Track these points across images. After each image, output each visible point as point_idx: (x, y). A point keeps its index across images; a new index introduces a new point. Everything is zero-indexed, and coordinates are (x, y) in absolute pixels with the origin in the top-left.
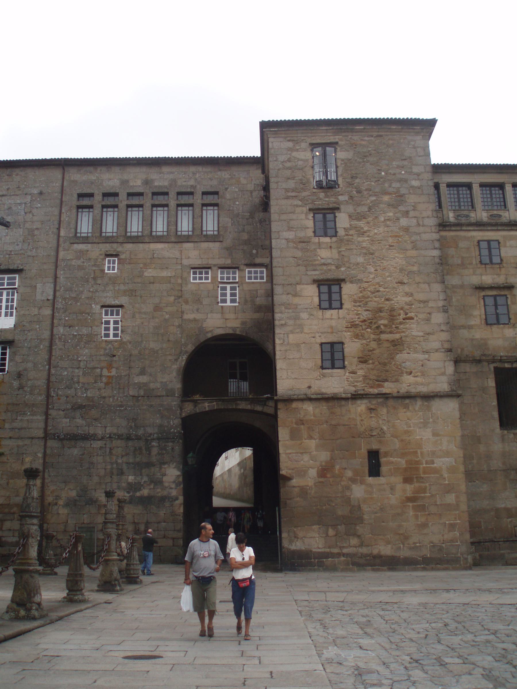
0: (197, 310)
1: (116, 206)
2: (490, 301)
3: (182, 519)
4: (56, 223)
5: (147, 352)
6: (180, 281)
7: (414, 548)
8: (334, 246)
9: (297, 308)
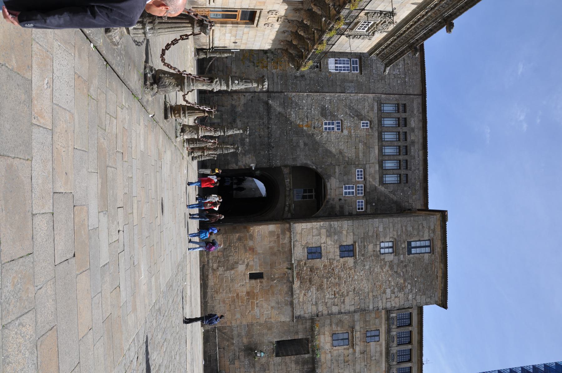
0: (341, 173)
1: (399, 126)
2: (346, 336)
4: (389, 92)
5: (317, 147)
6: (357, 163)
7: (212, 297)
8: (375, 253)
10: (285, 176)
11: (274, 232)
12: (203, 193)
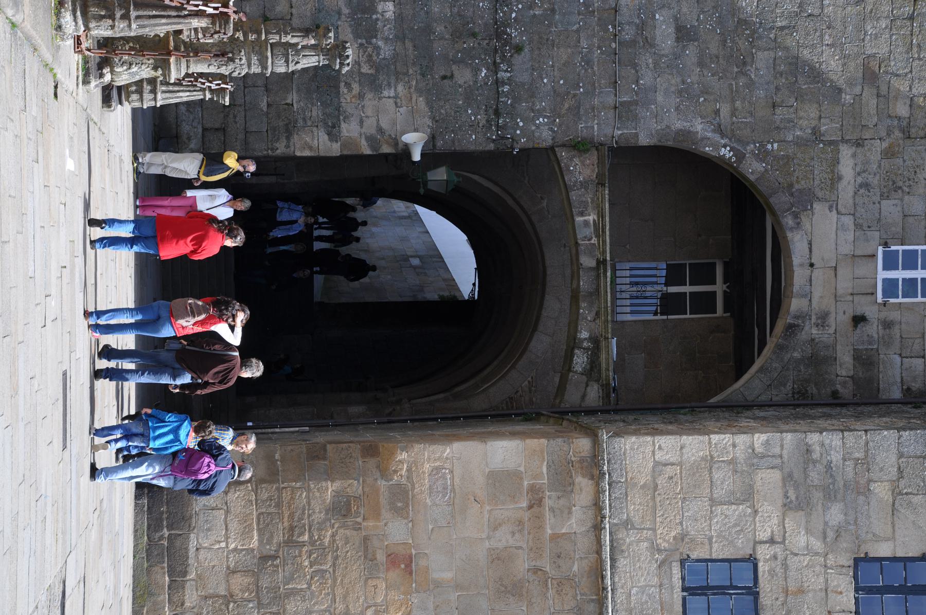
0: (866, 185)
3: (279, 152)
5: (743, 44)
9: (859, 493)
10: (574, 195)
11: (514, 476)
12: (163, 283)
